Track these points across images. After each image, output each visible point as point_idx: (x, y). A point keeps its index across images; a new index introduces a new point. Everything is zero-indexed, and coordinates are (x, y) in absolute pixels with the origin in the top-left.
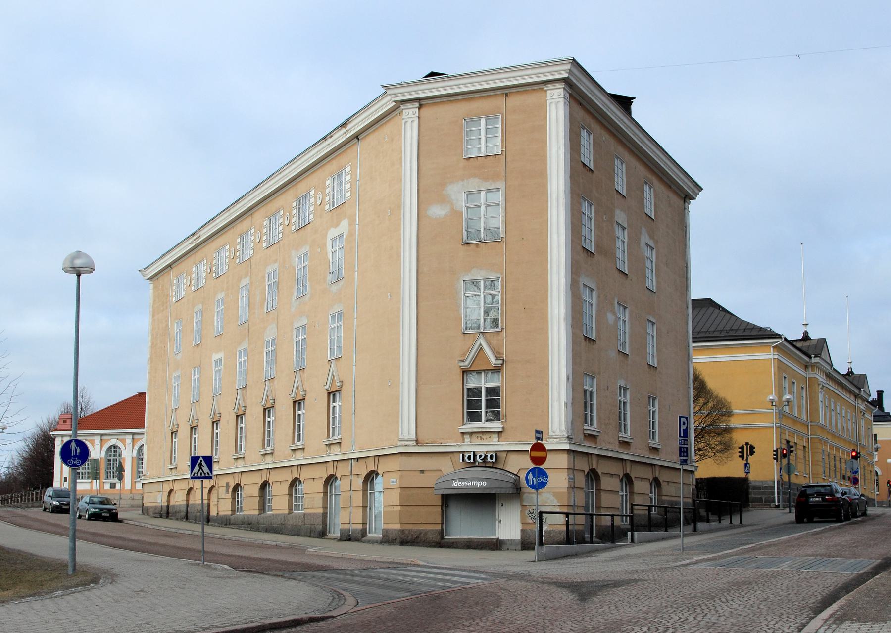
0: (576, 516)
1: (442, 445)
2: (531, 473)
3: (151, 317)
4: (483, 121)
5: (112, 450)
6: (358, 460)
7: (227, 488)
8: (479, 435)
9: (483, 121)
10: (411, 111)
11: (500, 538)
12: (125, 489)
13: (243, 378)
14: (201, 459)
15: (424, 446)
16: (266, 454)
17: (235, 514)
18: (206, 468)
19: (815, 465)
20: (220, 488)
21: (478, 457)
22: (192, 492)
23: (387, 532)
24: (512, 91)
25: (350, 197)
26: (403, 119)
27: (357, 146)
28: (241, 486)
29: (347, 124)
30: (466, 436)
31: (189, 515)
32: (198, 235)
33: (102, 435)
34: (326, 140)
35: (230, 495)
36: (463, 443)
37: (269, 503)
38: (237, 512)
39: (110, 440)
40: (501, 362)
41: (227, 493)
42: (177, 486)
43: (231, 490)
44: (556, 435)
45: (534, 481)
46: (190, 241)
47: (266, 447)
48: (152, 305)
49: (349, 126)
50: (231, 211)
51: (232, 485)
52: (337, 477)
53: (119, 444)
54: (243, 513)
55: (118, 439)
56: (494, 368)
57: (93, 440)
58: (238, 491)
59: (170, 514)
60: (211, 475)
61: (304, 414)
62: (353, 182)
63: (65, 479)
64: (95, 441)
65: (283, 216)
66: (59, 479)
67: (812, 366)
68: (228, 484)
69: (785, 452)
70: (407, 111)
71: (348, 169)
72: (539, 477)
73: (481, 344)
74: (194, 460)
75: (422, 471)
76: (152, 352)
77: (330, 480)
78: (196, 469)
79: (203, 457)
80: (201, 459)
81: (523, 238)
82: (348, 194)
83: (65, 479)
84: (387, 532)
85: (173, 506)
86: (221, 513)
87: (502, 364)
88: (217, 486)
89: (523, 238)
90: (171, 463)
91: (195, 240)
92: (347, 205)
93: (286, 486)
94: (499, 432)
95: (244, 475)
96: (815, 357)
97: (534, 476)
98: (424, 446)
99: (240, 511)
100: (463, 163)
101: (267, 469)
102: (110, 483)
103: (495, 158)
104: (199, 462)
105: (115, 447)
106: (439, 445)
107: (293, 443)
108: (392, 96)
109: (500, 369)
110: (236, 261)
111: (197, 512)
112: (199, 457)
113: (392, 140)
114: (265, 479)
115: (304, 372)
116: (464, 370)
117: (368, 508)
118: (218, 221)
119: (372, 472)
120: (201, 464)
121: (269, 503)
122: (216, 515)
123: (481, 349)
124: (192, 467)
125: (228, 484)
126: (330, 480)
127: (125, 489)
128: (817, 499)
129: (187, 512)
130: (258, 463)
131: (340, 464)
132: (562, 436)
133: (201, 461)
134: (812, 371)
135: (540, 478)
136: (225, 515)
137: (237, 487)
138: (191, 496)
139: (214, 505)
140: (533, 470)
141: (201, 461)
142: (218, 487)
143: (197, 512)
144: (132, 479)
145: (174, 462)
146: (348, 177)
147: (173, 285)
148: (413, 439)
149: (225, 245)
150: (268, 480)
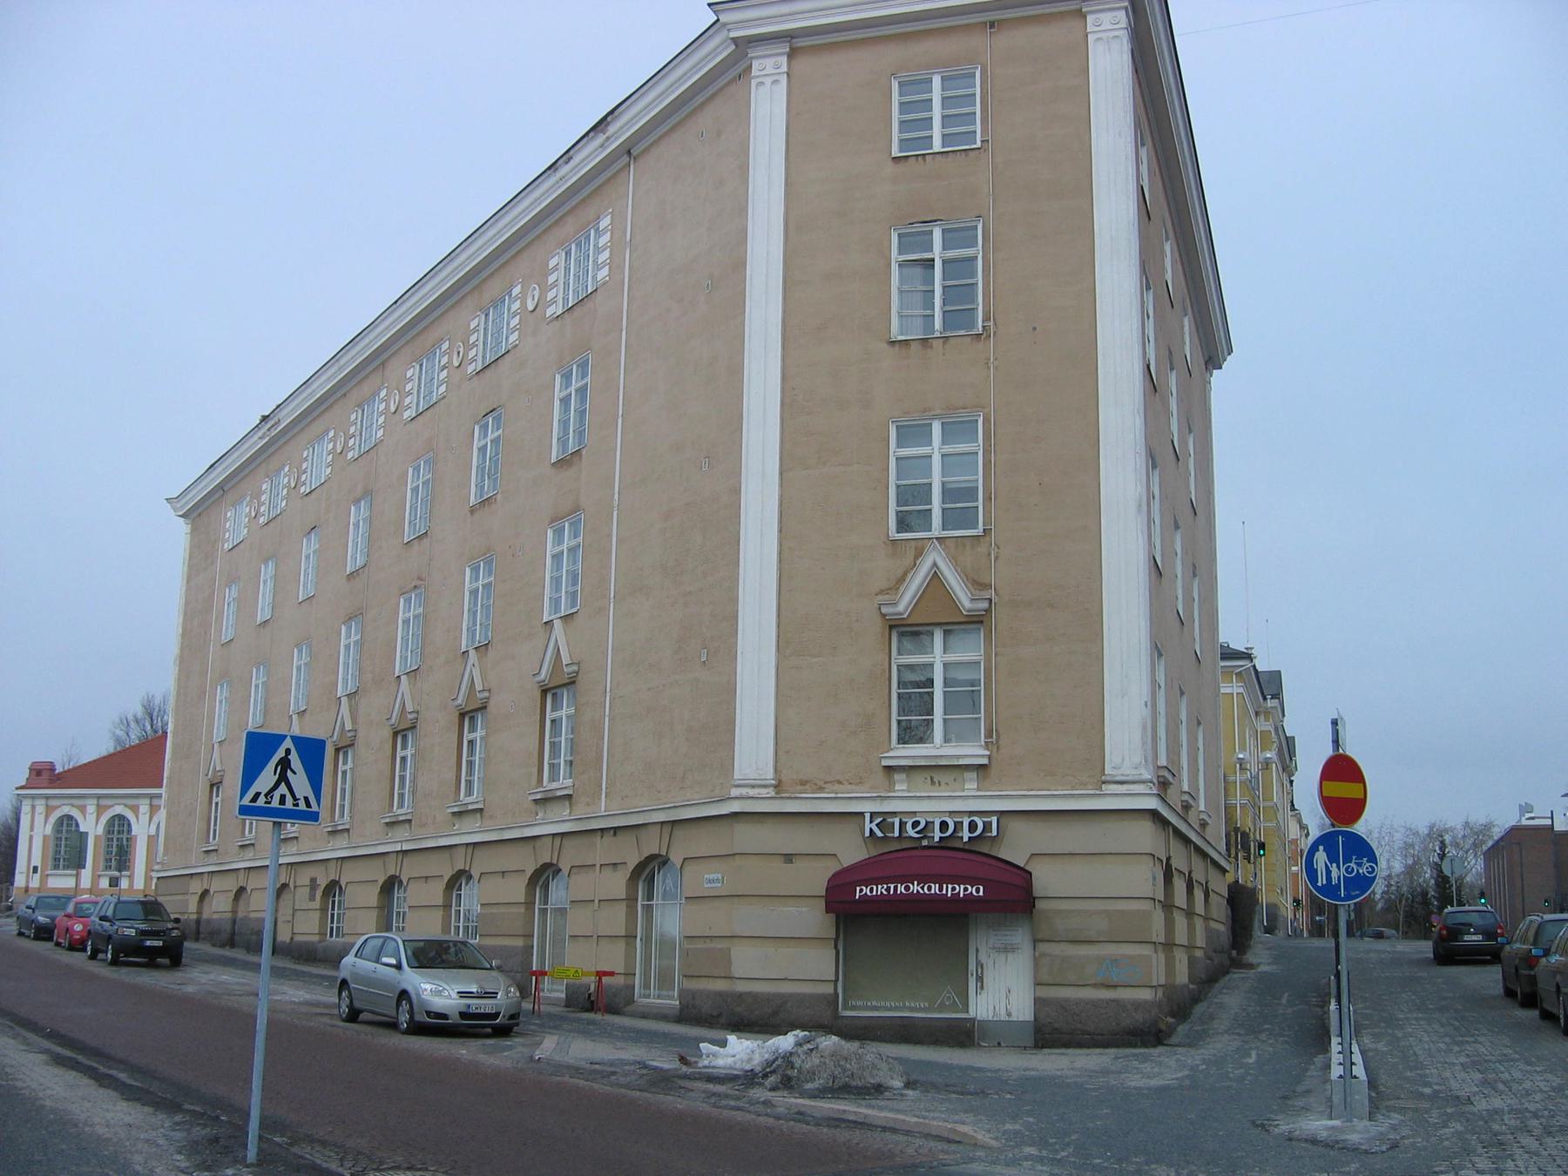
0: (25, 875)
1: (839, 795)
2: (1321, 848)
3: (185, 582)
4: (937, 81)
5: (116, 823)
6: (615, 834)
7: (311, 889)
8: (927, 774)
9: (937, 81)
10: (769, 64)
11: (979, 1018)
12: (135, 888)
13: (352, 674)
14: (288, 743)
15: (797, 798)
16: (393, 822)
17: (325, 940)
18: (300, 781)
19: (1522, 866)
20: (299, 890)
21: (909, 826)
22: (244, 896)
23: (693, 998)
24: (1006, 16)
25: (608, 278)
26: (753, 78)
27: (627, 173)
28: (341, 888)
29: (608, 124)
30: (897, 777)
31: (237, 938)
32: (276, 419)
33: (99, 797)
34: (555, 171)
35: (317, 904)
36: (963, 790)
37: (398, 922)
38: (331, 935)
39: (112, 806)
40: (985, 605)
41: (312, 898)
42: (216, 885)
43: (319, 894)
44: (1123, 775)
45: (1334, 874)
46: (260, 434)
47: (395, 808)
48: (187, 562)
49: (612, 129)
50: (342, 362)
51: (323, 883)
52: (471, 876)
53: (75, 813)
54: (343, 939)
55: (126, 806)
56: (967, 620)
57: (85, 806)
58: (334, 896)
59: (202, 936)
60: (315, 808)
61: (481, 738)
62: (614, 246)
63: (35, 869)
64: (88, 807)
65: (449, 352)
66: (25, 870)
67: (1265, 713)
68: (313, 880)
69: (1262, 852)
70: (761, 61)
71: (605, 222)
72: (1347, 860)
73: (935, 565)
74: (260, 747)
75: (789, 858)
76: (182, 643)
77: (390, 886)
78: (266, 779)
79: (295, 739)
80: (288, 743)
81: (1035, 329)
82: (605, 272)
83: (35, 869)
84: (693, 998)
85: (209, 921)
86: (298, 938)
87: (988, 611)
88: (292, 885)
89: (1035, 329)
90: (208, 842)
91: (269, 430)
92: (599, 297)
93: (438, 888)
94: (981, 768)
95: (347, 865)
96: (1271, 699)
97: (1332, 857)
98: (797, 798)
99: (337, 936)
100: (890, 169)
101: (398, 852)
102: (110, 879)
103: (966, 156)
104: (280, 753)
105: (121, 817)
106: (833, 795)
107: (457, 799)
108: (729, 27)
109: (982, 622)
110: (346, 456)
111: (251, 934)
112: (283, 738)
113: (719, 134)
114: (391, 872)
115: (487, 649)
116: (891, 623)
117: (638, 939)
118: (314, 386)
119: (546, 867)
120: (285, 764)
121: (398, 922)
122: (288, 941)
123: (935, 577)
124: (251, 772)
125: (313, 880)
126: (390, 886)
127: (135, 888)
128: (1474, 938)
129: (233, 934)
130: (377, 840)
131: (567, 842)
132: (1137, 778)
133: (288, 751)
134: (1265, 721)
135: (1352, 865)
136: (306, 943)
137: (333, 888)
138: (242, 903)
139: (284, 922)
140: (1327, 841)
141: (288, 751)
142: (295, 887)
143: (251, 934)
144: (146, 872)
145: (214, 838)
146: (605, 239)
147: (226, 520)
148: (768, 782)
149: (327, 432)
150: (398, 874)
